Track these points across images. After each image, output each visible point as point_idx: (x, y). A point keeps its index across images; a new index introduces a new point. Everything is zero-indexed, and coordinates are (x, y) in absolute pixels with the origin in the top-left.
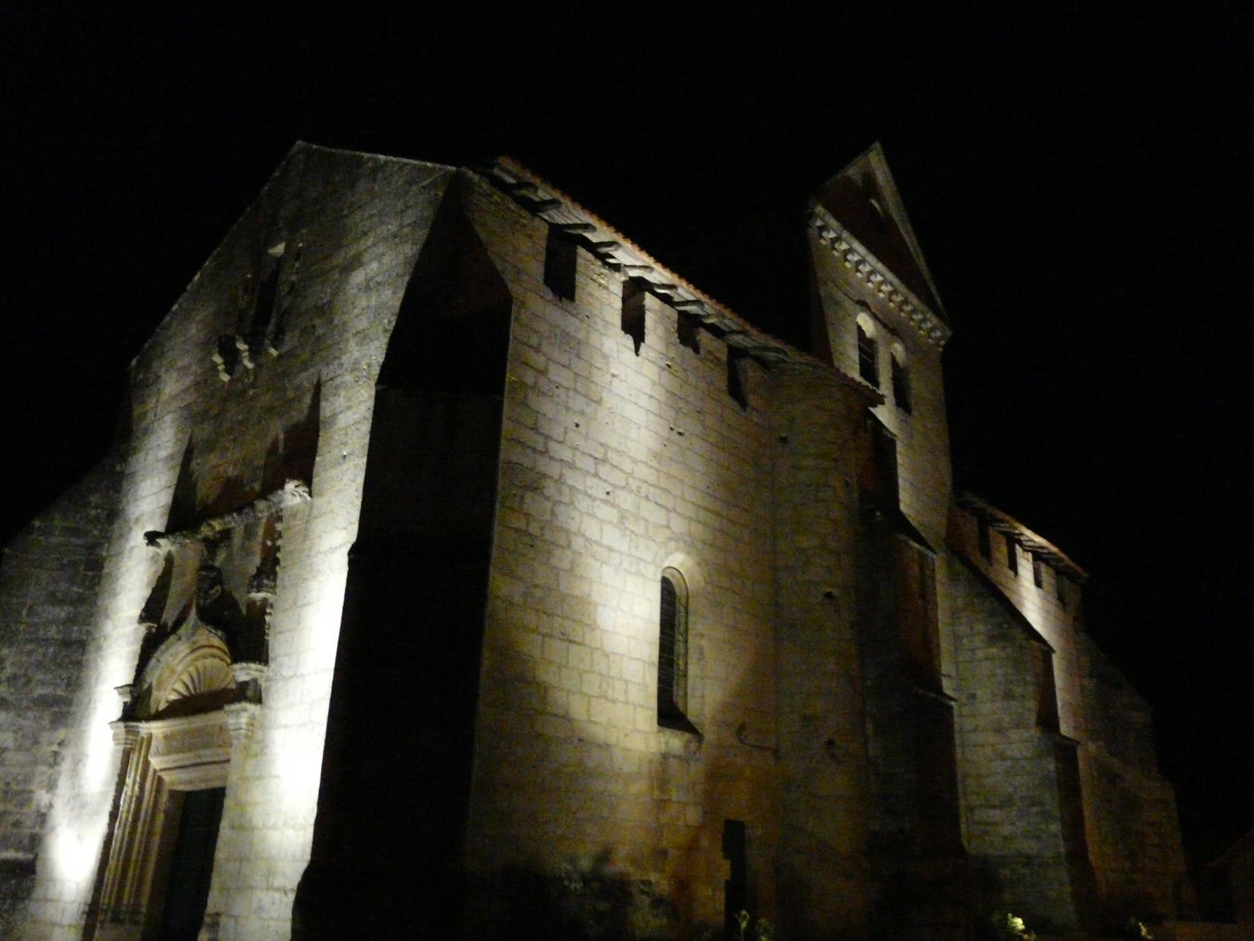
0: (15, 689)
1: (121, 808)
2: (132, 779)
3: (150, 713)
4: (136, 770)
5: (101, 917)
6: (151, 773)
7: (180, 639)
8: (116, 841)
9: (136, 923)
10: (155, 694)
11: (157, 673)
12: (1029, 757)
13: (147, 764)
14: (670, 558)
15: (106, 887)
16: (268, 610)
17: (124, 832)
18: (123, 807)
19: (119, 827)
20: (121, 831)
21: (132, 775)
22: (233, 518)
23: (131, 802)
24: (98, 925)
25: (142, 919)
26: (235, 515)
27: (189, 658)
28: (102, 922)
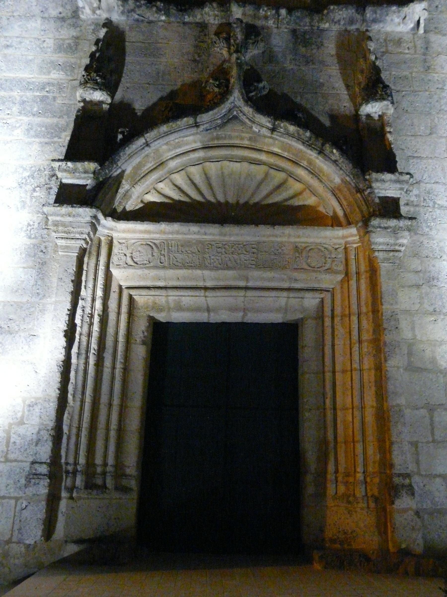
0: (42, 130)
1: (78, 329)
2: (90, 291)
3: (377, 203)
4: (95, 279)
5: (67, 482)
6: (114, 288)
7: (197, 125)
8: (76, 372)
9: (125, 490)
10: (125, 186)
11: (136, 161)
12: (396, 552)
13: (108, 276)
14: (65, 174)
15: (69, 438)
16: (388, 129)
17: (86, 363)
18: (81, 327)
19: (79, 354)
20: (82, 361)
21: (90, 285)
22: (278, 14)
23: (91, 324)
24: (64, 494)
25: (133, 484)
26: (283, 12)
27: (201, 154)
28: (70, 490)
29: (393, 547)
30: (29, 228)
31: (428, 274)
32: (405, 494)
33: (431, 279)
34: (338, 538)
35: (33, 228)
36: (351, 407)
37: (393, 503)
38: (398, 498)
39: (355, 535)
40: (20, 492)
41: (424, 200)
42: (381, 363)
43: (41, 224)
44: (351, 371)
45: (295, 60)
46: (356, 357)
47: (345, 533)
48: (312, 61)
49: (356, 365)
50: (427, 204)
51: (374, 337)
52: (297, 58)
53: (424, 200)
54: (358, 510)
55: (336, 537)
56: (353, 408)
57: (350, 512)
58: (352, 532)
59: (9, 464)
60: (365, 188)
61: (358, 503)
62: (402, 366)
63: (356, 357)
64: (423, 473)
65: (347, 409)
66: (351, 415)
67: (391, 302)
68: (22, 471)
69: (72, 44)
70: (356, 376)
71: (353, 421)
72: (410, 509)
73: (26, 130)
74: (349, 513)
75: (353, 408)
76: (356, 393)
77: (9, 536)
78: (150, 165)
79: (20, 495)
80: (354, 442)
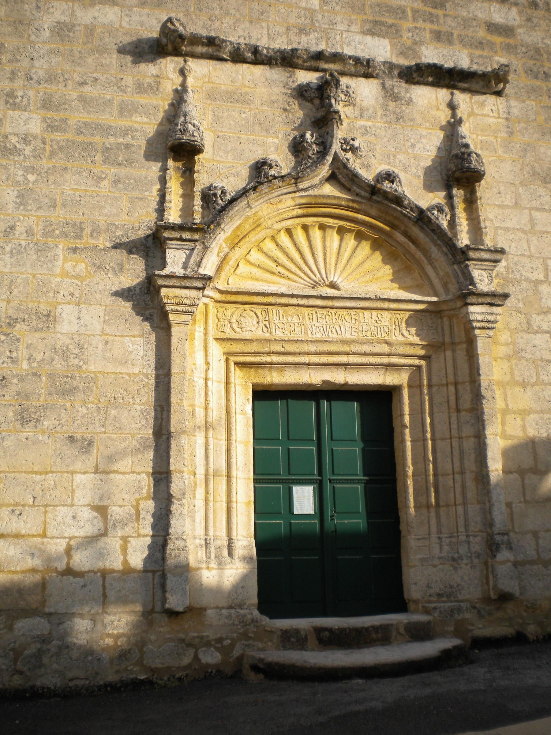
29: (495, 594)
30: (131, 293)
31: (518, 346)
32: (504, 549)
33: (520, 351)
34: (445, 592)
35: (135, 294)
36: (451, 472)
37: (495, 556)
38: (499, 552)
39: (460, 588)
40: (156, 566)
41: (513, 271)
42: (479, 431)
43: (143, 289)
44: (451, 438)
45: (386, 115)
46: (454, 426)
47: (451, 587)
48: (402, 117)
49: (454, 432)
50: (514, 275)
51: (472, 406)
52: (388, 113)
53: (513, 271)
54: (463, 566)
55: (442, 592)
56: (453, 474)
57: (455, 569)
58: (457, 586)
59: (142, 539)
60: (462, 260)
61: (462, 560)
62: (70, 364)
63: (454, 426)
64: (517, 530)
65: (448, 475)
66: (452, 481)
67: (488, 374)
68: (155, 546)
69: (153, 84)
70: (455, 443)
71: (454, 485)
72: (508, 561)
73: (113, 181)
74: (454, 569)
75: (453, 474)
76: (456, 460)
77: (151, 607)
78: (247, 227)
79: (157, 569)
80: (455, 505)
